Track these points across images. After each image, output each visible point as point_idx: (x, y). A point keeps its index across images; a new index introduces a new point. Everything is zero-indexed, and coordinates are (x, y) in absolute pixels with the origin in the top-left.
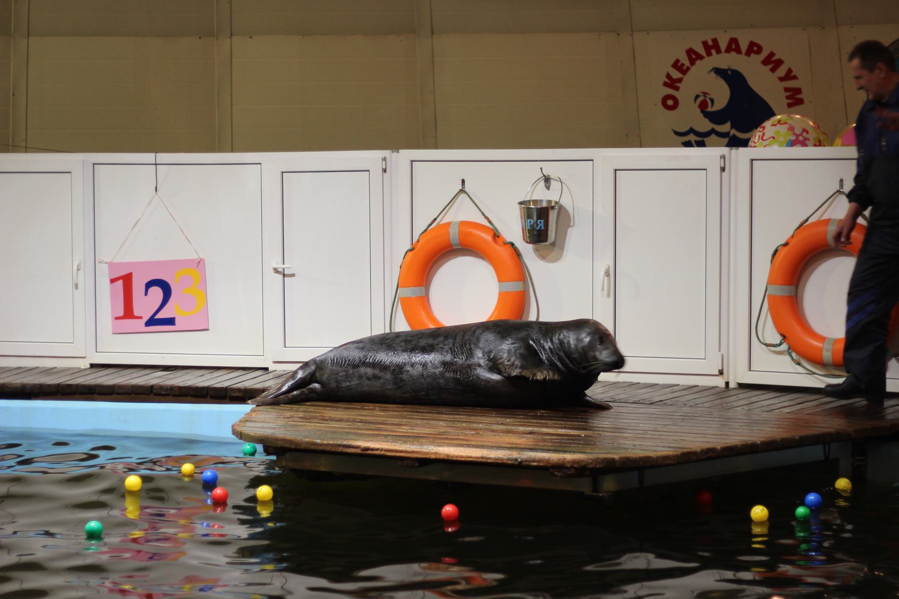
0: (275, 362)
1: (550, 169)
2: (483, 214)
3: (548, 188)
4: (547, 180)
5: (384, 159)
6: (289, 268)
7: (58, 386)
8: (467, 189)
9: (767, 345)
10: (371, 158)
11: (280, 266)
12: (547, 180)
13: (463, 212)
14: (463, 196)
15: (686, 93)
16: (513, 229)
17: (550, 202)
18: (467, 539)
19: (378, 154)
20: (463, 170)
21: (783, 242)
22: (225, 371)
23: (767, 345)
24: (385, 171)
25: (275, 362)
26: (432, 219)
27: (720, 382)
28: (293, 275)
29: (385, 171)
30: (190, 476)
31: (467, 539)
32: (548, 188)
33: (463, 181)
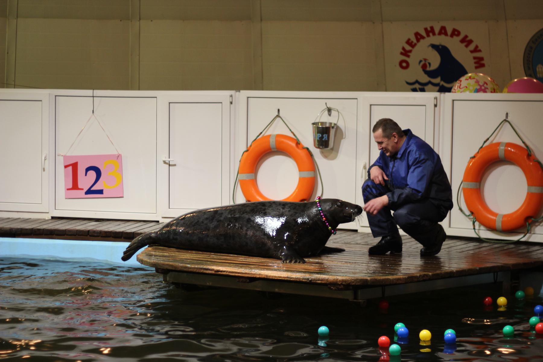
0: (163, 218)
3: (330, 115)
4: (329, 110)
5: (231, 96)
6: (172, 161)
8: (281, 115)
10: (223, 95)
11: (167, 160)
12: (329, 110)
14: (278, 119)
24: (231, 103)
25: (163, 218)
29: (231, 103)
32: (330, 115)
33: (279, 110)
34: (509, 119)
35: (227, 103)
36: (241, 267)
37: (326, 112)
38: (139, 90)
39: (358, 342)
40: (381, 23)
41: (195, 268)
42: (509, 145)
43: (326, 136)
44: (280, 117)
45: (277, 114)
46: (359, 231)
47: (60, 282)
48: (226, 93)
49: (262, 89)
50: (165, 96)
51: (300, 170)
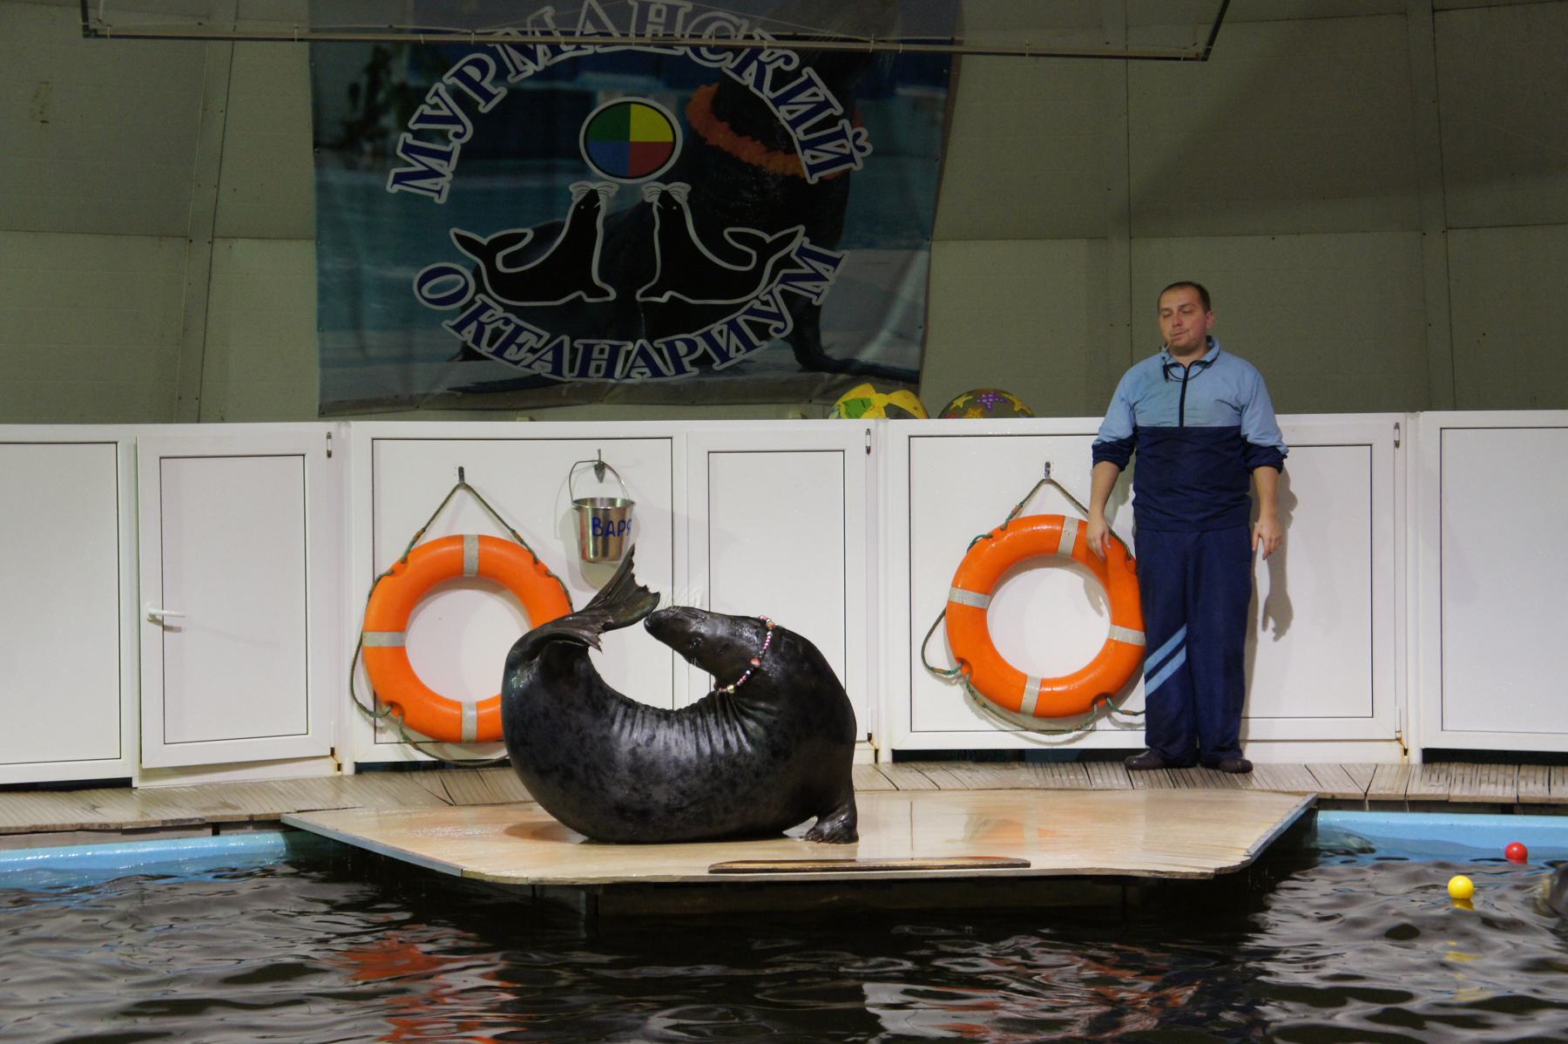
3: (601, 479)
4: (600, 468)
5: (1397, 426)
6: (169, 614)
7: (1429, 811)
8: (467, 481)
9: (932, 670)
11: (157, 611)
12: (600, 468)
13: (469, 522)
14: (1046, 487)
15: (517, 358)
19: (1387, 419)
21: (539, 556)
23: (932, 670)
24: (1397, 444)
26: (419, 529)
28: (178, 630)
29: (1397, 444)
30: (1466, 901)
32: (601, 479)
33: (461, 470)
34: (1053, 476)
36: (29, 845)
37: (592, 473)
38: (199, 421)
39: (894, 964)
41: (93, 857)
42: (483, 539)
44: (468, 488)
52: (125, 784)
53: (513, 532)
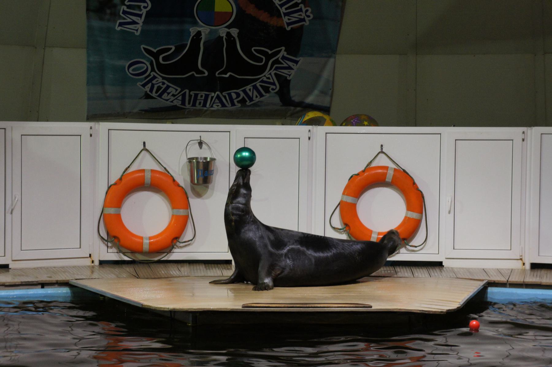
0: (447, 258)
1: (205, 137)
2: (129, 167)
3: (201, 148)
4: (201, 144)
8: (147, 147)
10: (515, 132)
13: (147, 164)
14: (381, 155)
16: (182, 176)
17: (206, 158)
18: (315, 340)
19: (520, 130)
20: (144, 136)
22: (202, 267)
24: (523, 140)
25: (447, 258)
27: (88, 262)
29: (309, 138)
31: (315, 340)
32: (201, 148)
34: (384, 150)
35: (304, 139)
40: (44, 49)
42: (152, 171)
43: (203, 172)
44: (147, 150)
45: (142, 147)
46: (10, 267)
47: (419, 344)
48: (518, 130)
49: (416, 125)
50: (450, 133)
51: (173, 208)
52: (439, 264)
53: (165, 168)
